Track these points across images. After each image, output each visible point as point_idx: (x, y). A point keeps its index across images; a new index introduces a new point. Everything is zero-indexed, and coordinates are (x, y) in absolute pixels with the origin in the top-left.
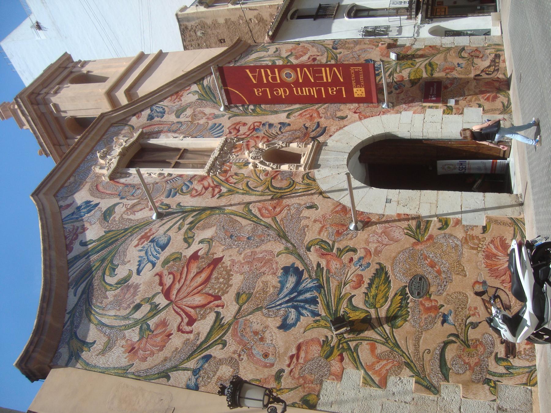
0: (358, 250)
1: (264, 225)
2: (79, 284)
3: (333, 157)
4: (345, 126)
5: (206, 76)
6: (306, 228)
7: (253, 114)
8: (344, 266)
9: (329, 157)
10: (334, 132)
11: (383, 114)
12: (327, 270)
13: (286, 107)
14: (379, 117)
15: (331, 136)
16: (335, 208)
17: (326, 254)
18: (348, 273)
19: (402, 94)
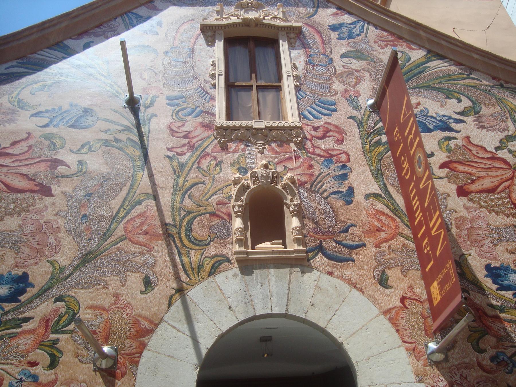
0: (53, 371)
1: (109, 229)
2: (23, 65)
3: (274, 290)
4: (361, 291)
5: (451, 60)
6: (101, 286)
7: (367, 147)
8: (22, 356)
9: (273, 283)
10: (341, 277)
11: (407, 349)
12: (17, 333)
13: (394, 186)
14: (399, 342)
15: (330, 274)
16: (145, 318)
17: (47, 326)
18: (8, 364)
19: (481, 373)
